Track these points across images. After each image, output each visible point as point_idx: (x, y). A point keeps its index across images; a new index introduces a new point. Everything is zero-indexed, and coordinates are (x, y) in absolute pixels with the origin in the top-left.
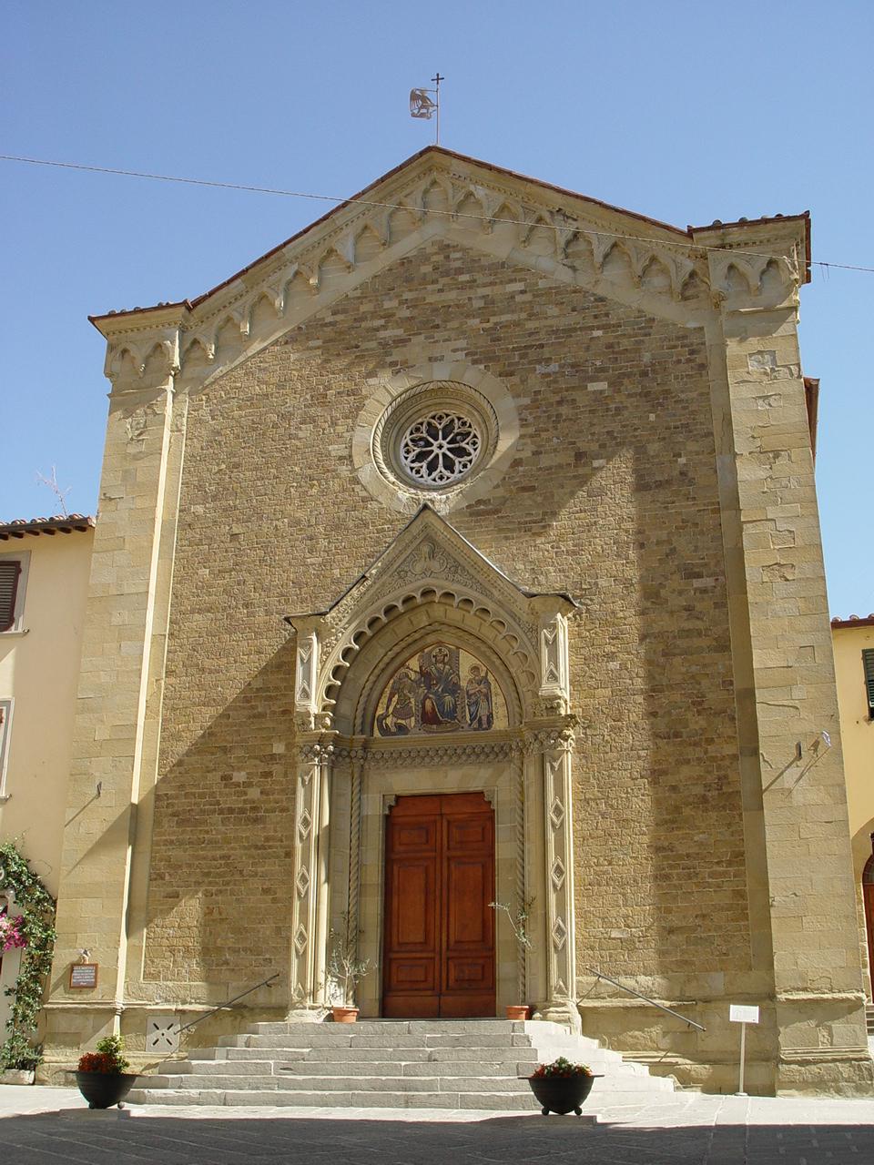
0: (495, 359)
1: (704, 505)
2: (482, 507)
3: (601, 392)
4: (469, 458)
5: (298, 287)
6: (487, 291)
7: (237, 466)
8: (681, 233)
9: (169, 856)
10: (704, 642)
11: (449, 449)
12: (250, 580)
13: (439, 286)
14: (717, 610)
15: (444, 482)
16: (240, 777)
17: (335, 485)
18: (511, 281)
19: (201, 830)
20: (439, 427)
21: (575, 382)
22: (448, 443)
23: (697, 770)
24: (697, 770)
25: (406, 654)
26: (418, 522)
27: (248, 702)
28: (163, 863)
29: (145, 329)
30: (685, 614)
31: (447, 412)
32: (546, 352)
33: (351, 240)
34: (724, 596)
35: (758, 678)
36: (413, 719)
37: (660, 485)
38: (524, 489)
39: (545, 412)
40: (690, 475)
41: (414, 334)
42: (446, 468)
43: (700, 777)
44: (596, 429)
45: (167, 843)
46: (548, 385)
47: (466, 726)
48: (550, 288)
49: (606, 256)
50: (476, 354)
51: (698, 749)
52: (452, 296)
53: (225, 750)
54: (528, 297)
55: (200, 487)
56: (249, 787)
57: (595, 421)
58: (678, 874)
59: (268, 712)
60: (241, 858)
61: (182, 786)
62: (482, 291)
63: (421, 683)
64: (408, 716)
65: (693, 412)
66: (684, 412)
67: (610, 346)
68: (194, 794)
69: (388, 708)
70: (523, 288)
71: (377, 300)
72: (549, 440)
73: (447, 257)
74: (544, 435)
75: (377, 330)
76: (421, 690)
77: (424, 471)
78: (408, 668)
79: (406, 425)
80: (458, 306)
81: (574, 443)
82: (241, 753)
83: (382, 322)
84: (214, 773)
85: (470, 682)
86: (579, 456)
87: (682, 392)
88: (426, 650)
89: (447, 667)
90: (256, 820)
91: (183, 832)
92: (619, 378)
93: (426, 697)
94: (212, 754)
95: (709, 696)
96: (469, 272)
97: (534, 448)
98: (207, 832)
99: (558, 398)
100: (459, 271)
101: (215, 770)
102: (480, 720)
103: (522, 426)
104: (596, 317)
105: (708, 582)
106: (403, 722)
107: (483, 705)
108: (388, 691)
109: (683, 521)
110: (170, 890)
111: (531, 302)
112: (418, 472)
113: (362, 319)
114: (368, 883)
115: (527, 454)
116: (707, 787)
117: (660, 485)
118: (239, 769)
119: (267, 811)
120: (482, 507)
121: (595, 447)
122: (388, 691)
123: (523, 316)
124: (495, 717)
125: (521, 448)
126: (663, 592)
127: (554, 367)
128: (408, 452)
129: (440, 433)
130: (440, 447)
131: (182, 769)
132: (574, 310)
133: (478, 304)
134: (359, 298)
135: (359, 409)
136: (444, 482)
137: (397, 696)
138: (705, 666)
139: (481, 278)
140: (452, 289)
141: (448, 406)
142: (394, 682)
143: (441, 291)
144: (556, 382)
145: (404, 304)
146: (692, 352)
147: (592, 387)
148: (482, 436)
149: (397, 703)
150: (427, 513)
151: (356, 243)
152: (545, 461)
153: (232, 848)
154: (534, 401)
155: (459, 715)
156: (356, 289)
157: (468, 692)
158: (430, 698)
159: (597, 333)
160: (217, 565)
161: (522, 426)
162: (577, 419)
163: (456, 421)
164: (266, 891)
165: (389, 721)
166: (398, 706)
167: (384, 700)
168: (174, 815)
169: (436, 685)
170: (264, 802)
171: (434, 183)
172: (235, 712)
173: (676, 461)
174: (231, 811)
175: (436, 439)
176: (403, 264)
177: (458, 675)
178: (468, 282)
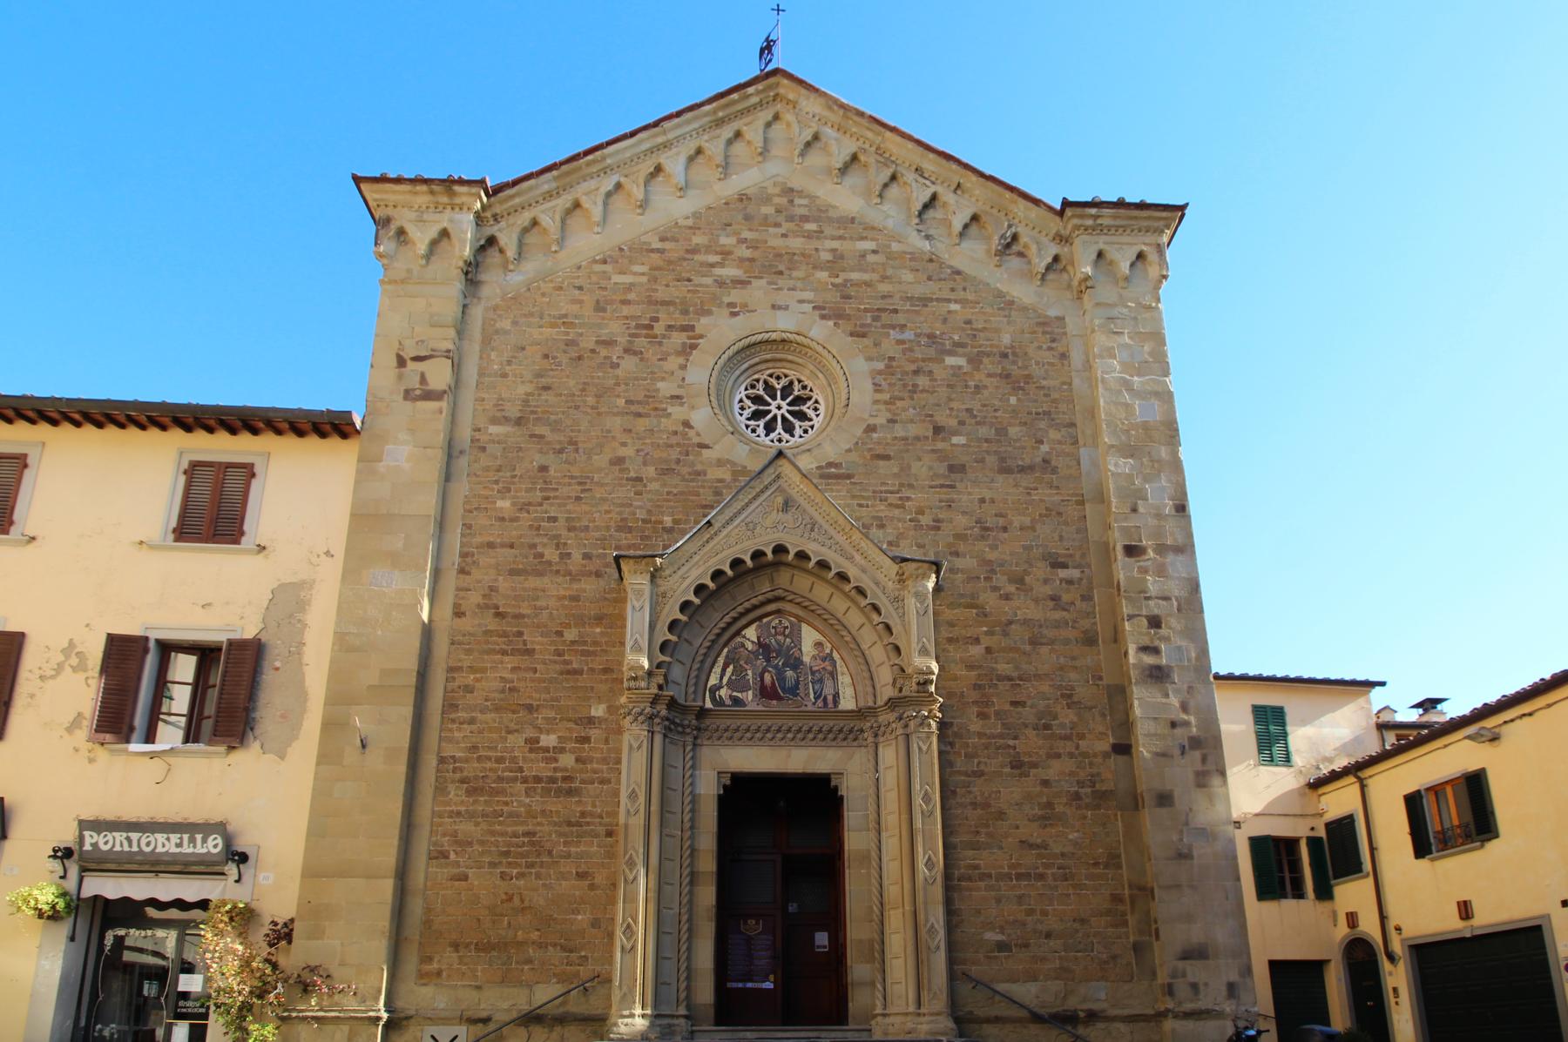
0: (848, 318)
1: (1068, 495)
2: (833, 470)
3: (960, 367)
4: (811, 423)
5: (618, 201)
6: (835, 244)
7: (546, 388)
8: (1050, 208)
9: (456, 831)
10: (1069, 633)
11: (788, 411)
14: (1085, 603)
16: (549, 740)
18: (865, 238)
19: (498, 801)
20: (777, 386)
21: (932, 352)
22: (789, 404)
23: (1068, 765)
24: (1068, 765)
25: (743, 621)
26: (770, 470)
27: (559, 655)
28: (447, 838)
29: (427, 207)
30: (1051, 604)
33: (682, 160)
34: (1091, 589)
36: (750, 692)
37: (1022, 470)
39: (900, 380)
40: (1053, 463)
41: (756, 277)
42: (786, 431)
43: (1071, 774)
44: (954, 405)
45: (452, 814)
46: (904, 353)
47: (809, 704)
48: (905, 253)
49: (966, 226)
50: (824, 308)
51: (1069, 743)
52: (796, 243)
53: (530, 708)
55: (498, 406)
56: (561, 753)
57: (954, 396)
58: (1053, 874)
59: (585, 668)
60: (550, 835)
61: (474, 748)
63: (759, 654)
64: (745, 689)
65: (1054, 401)
66: (1045, 399)
67: (968, 322)
68: (489, 758)
69: (721, 678)
70: (874, 248)
71: (712, 234)
72: (904, 410)
73: (791, 202)
74: (899, 404)
75: (712, 265)
76: (759, 662)
79: (742, 378)
80: (803, 255)
81: (931, 416)
82: (552, 714)
83: (717, 258)
84: (516, 734)
85: (814, 657)
86: (938, 430)
87: (1044, 379)
88: (765, 620)
89: (788, 640)
90: (570, 792)
91: (475, 802)
92: (978, 355)
93: (764, 670)
94: (514, 712)
95: (1078, 690)
96: (816, 220)
97: (889, 416)
98: (506, 804)
99: (913, 367)
100: (804, 219)
101: (517, 731)
102: (825, 699)
103: (876, 391)
104: (953, 290)
105: (1073, 573)
106: (739, 695)
108: (721, 660)
109: (1047, 509)
110: (456, 871)
111: (883, 264)
112: (754, 431)
113: (694, 251)
114: (701, 870)
115: (881, 420)
116: (1081, 784)
117: (1022, 470)
118: (548, 732)
119: (583, 782)
120: (833, 470)
121: (953, 423)
122: (721, 660)
123: (875, 277)
125: (875, 413)
126: (1027, 579)
127: (908, 335)
128: (742, 408)
129: (779, 393)
131: (474, 727)
132: (929, 279)
133: (826, 256)
134: (690, 228)
135: (694, 347)
137: (731, 667)
138: (1073, 658)
139: (828, 231)
140: (798, 236)
141: (788, 365)
142: (729, 651)
143: (784, 236)
144: (911, 350)
145: (743, 243)
146: (1053, 341)
147: (950, 361)
148: (826, 400)
149: (732, 674)
150: (782, 462)
151: (687, 168)
153: (539, 824)
154: (888, 367)
155: (801, 691)
156: (688, 218)
157: (811, 668)
158: (769, 671)
159: (954, 307)
160: (524, 496)
161: (876, 391)
162: (935, 392)
163: (796, 383)
164: (581, 876)
165: (723, 692)
166: (734, 678)
167: (717, 669)
168: (462, 781)
169: (776, 658)
170: (581, 771)
171: (776, 117)
172: (542, 666)
173: (1039, 448)
174: (538, 779)
175: (783, 399)
176: (741, 200)
177: (800, 649)
178: (815, 232)
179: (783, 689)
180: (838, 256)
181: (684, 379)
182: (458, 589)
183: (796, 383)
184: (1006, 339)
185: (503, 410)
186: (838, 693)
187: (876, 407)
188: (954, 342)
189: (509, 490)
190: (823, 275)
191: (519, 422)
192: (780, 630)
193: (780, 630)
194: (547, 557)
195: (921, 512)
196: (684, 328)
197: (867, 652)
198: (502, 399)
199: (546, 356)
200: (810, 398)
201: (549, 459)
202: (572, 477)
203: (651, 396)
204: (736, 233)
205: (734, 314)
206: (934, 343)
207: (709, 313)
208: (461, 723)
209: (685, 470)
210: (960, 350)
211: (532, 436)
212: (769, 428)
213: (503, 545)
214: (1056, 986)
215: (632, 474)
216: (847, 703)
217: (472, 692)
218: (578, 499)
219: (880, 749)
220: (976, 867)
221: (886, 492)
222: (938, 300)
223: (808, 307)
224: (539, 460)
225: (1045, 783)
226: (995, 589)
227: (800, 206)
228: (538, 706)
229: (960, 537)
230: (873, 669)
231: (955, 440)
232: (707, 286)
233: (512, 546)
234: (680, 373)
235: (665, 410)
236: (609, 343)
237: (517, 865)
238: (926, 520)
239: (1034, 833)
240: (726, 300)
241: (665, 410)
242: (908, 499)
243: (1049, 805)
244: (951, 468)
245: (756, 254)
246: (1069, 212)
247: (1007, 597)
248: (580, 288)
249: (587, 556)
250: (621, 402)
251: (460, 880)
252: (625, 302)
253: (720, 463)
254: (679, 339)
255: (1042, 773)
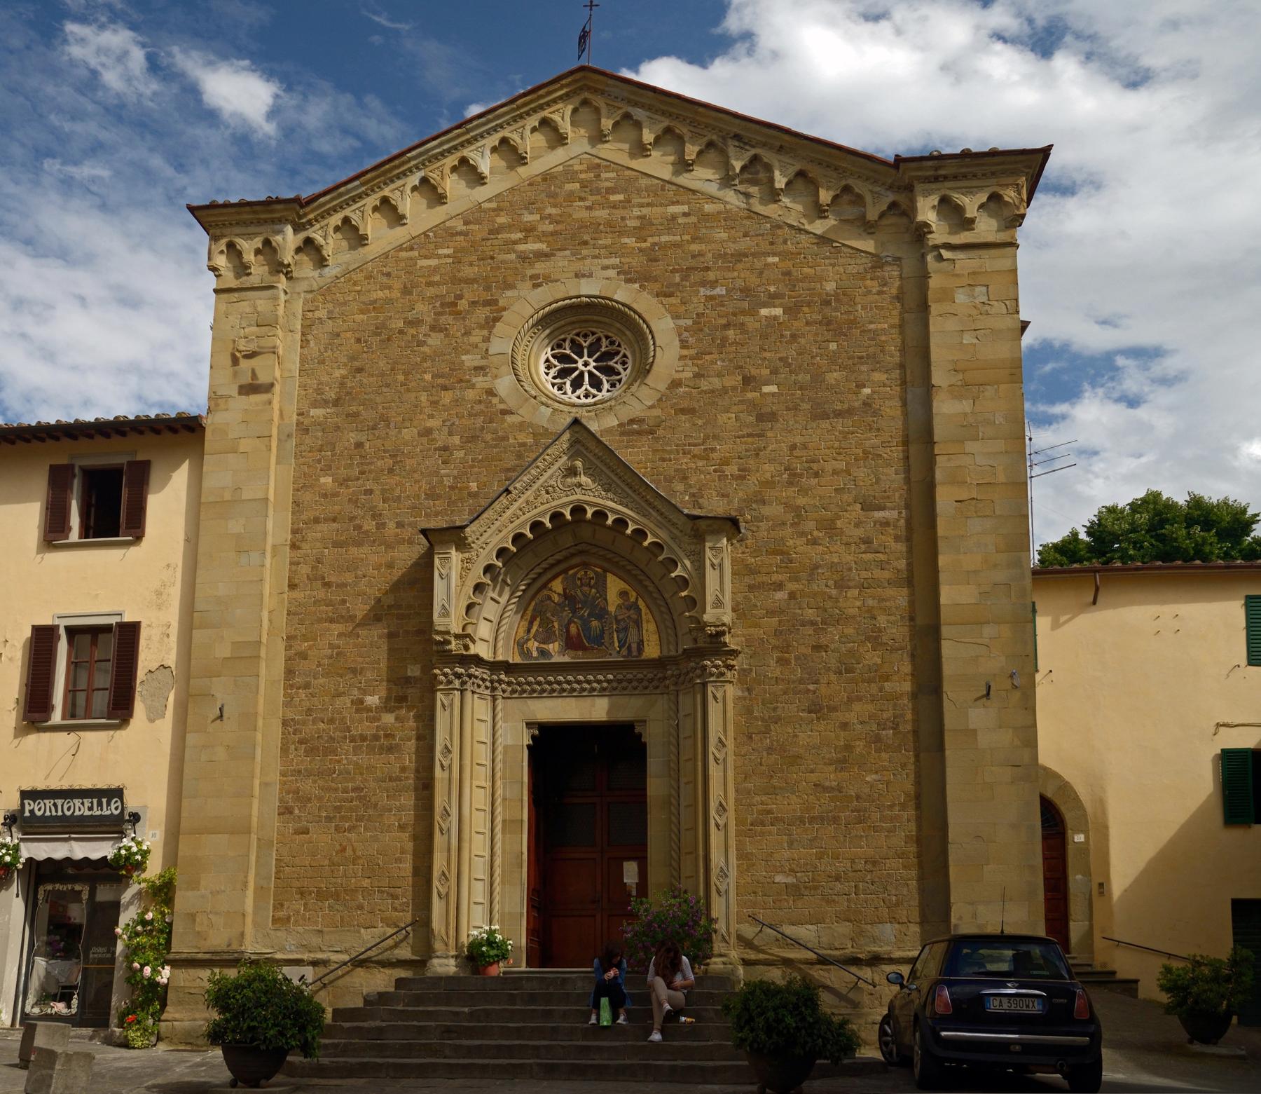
0: (655, 280)
3: (775, 318)
4: (619, 377)
7: (360, 370)
11: (595, 367)
12: (377, 489)
13: (587, 203)
15: (590, 400)
17: (470, 394)
18: (673, 203)
20: (584, 344)
25: (549, 575)
31: (594, 330)
32: (711, 276)
35: (945, 615)
38: (683, 411)
39: (709, 335)
41: (560, 250)
47: (614, 653)
52: (602, 214)
53: (354, 671)
54: (693, 219)
55: (319, 391)
62: (636, 212)
63: (565, 606)
67: (788, 273)
75: (515, 243)
76: (565, 613)
77: (568, 387)
78: (551, 590)
83: (520, 235)
85: (619, 607)
86: (747, 381)
88: (571, 572)
89: (593, 590)
90: (390, 749)
93: (570, 622)
96: (625, 191)
99: (724, 321)
100: (610, 191)
102: (629, 648)
107: (633, 631)
116: (882, 726)
117: (839, 414)
124: (645, 644)
125: (681, 369)
126: (839, 524)
127: (720, 291)
130: (586, 364)
132: (745, 235)
133: (631, 223)
135: (496, 320)
136: (590, 400)
137: (538, 619)
142: (536, 604)
145: (547, 218)
152: (704, 385)
154: (695, 323)
158: (575, 622)
160: (343, 472)
161: (683, 347)
163: (604, 340)
168: (301, 742)
169: (582, 608)
174: (363, 738)
177: (606, 600)
179: (588, 639)
180: (645, 222)
181: (487, 350)
182: (291, 563)
183: (604, 340)
184: (830, 287)
185: (323, 393)
186: (642, 641)
187: (682, 363)
188: (770, 294)
189: (330, 468)
190: (629, 241)
191: (336, 403)
192: (586, 581)
193: (586, 581)
194: (365, 527)
195: (725, 462)
196: (487, 303)
197: (669, 601)
198: (322, 384)
199: (358, 341)
200: (618, 353)
201: (362, 437)
202: (385, 451)
203: (456, 367)
204: (539, 210)
205: (536, 286)
206: (747, 296)
207: (511, 287)
208: (299, 688)
209: (489, 437)
210: (777, 302)
211: (348, 415)
212: (577, 384)
213: (326, 520)
214: (844, 928)
215: (439, 444)
216: (652, 650)
217: (306, 659)
218: (391, 471)
219: (681, 697)
220: (769, 812)
221: (690, 445)
222: (753, 255)
223: (612, 273)
224: (353, 437)
225: (845, 726)
226: (803, 534)
227: (607, 179)
228: (362, 669)
229: (769, 484)
230: (675, 617)
231: (766, 389)
232: (512, 262)
233: (334, 520)
234: (484, 345)
235: (469, 381)
236: (416, 323)
237: (350, 819)
238: (732, 469)
239: (831, 777)
240: (529, 272)
241: (469, 381)
242: (713, 450)
243: (848, 748)
244: (760, 418)
245: (560, 227)
246: (902, 165)
247: (814, 542)
248: (388, 275)
249: (400, 525)
250: (428, 377)
251: (302, 833)
252: (429, 284)
253: (522, 426)
254: (482, 313)
255: (839, 716)
